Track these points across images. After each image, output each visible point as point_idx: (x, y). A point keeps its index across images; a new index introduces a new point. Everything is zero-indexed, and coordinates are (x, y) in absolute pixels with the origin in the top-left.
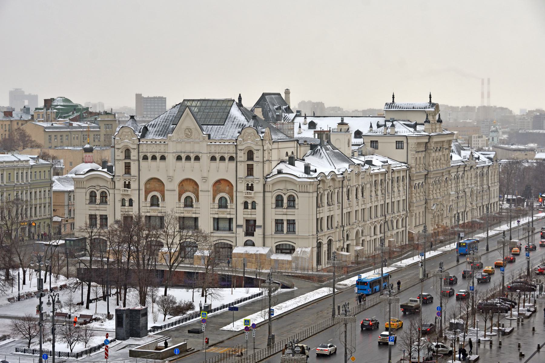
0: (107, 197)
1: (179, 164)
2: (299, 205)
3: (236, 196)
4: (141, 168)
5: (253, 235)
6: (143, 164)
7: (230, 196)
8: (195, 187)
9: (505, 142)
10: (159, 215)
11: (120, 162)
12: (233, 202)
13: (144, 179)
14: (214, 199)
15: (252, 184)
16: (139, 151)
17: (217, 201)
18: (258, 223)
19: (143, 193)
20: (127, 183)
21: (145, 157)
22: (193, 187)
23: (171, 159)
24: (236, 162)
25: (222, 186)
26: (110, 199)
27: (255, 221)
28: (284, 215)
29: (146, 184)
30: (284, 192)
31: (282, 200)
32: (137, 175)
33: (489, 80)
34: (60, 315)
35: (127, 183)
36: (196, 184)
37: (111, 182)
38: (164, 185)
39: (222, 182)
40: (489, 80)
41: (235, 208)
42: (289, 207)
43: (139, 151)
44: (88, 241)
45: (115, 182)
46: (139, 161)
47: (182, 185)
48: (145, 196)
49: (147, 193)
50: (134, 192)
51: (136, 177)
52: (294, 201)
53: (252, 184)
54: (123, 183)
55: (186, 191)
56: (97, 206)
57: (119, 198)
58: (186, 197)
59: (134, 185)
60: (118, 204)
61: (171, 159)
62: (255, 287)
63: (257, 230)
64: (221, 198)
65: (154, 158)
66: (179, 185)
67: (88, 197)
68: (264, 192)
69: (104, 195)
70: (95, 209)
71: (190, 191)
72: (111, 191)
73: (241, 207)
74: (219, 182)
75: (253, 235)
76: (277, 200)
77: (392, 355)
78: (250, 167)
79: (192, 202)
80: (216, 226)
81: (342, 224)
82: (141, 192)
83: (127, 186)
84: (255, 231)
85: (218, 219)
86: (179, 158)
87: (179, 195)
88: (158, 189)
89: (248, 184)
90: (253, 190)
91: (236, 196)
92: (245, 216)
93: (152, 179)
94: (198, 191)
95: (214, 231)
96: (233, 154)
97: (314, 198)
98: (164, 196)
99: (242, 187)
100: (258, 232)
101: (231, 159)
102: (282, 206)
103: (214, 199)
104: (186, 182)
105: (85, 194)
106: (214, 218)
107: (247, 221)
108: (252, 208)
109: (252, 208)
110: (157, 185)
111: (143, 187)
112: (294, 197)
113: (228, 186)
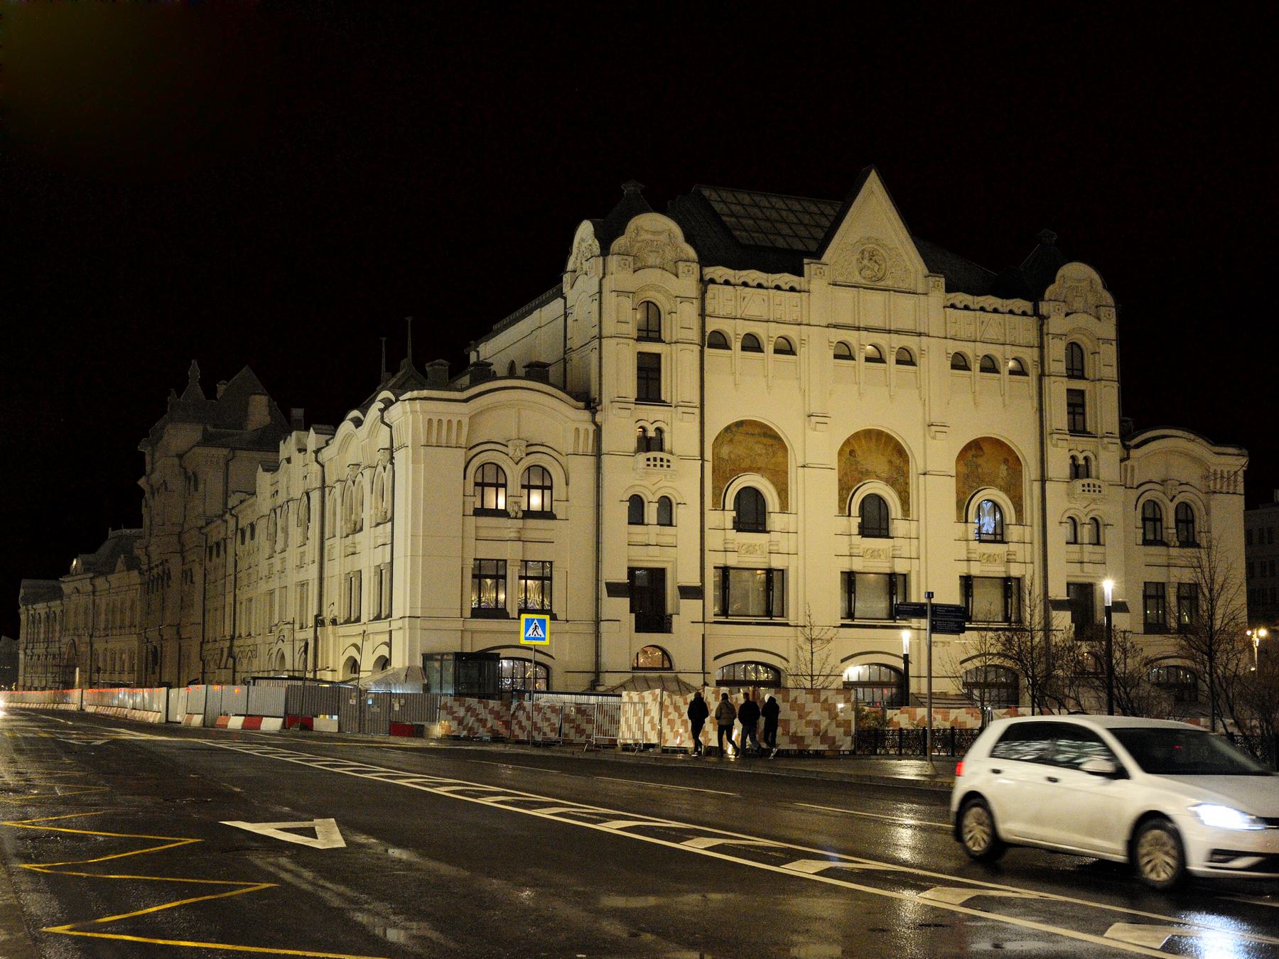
8: (897, 461)
9: (520, 371)
13: (717, 422)
16: (703, 308)
22: (890, 462)
25: (987, 464)
34: (636, 766)
36: (900, 451)
43: (703, 308)
44: (929, 605)
47: (852, 452)
49: (723, 474)
53: (659, 430)
55: (865, 474)
62: (1183, 774)
65: (752, 344)
66: (840, 453)
71: (878, 477)
74: (975, 447)
87: (841, 489)
88: (761, 462)
94: (905, 475)
97: (529, 535)
110: (759, 449)
113: (1006, 461)
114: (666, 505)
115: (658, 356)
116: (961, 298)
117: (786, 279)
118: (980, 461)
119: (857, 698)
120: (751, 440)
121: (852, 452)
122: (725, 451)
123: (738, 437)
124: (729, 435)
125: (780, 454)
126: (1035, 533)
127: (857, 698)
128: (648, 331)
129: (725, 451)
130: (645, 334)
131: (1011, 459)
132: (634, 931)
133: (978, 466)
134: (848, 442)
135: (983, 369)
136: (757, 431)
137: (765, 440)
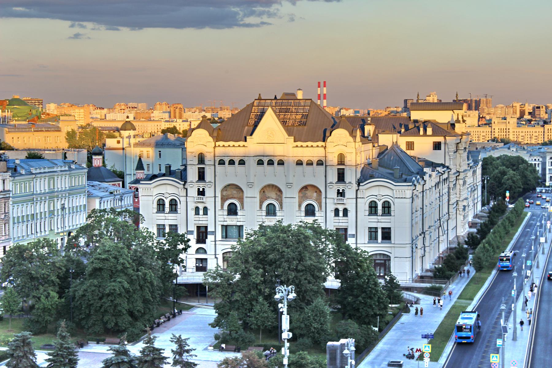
0: (177, 205)
1: (260, 167)
2: (395, 211)
3: (326, 203)
4: (216, 174)
5: (204, 242)
6: (219, 168)
7: (318, 203)
8: (279, 193)
10: (238, 225)
11: (194, 167)
12: (321, 208)
14: (300, 206)
15: (203, 189)
17: (303, 208)
18: (209, 229)
19: (219, 200)
20: (201, 190)
21: (270, 162)
22: (276, 194)
23: (252, 163)
24: (326, 166)
25: (309, 193)
26: (181, 207)
27: (206, 227)
28: (380, 222)
29: (222, 191)
30: (379, 198)
31: (164, 205)
32: (213, 181)
33: (325, 82)
35: (201, 190)
36: (280, 191)
37: (183, 189)
38: (242, 191)
39: (309, 188)
40: (325, 82)
41: (324, 216)
42: (384, 214)
45: (187, 189)
46: (215, 165)
47: (264, 192)
48: (221, 203)
49: (223, 200)
50: (208, 199)
51: (211, 184)
52: (176, 205)
53: (203, 189)
54: (197, 190)
56: (379, 217)
57: (192, 206)
58: (268, 204)
59: (209, 192)
60: (192, 213)
61: (252, 163)
63: (208, 236)
64: (230, 204)
66: (260, 192)
67: (155, 205)
68: (357, 198)
69: (174, 203)
70: (164, 218)
71: (272, 198)
72: (183, 199)
73: (331, 214)
74: (305, 188)
75: (204, 242)
76: (370, 207)
77: (505, 363)
78: (202, 171)
79: (236, 209)
80: (224, 234)
81: (423, 230)
82: (217, 198)
83: (201, 193)
84: (206, 238)
85: (226, 226)
86: (260, 163)
87: (260, 202)
88: (235, 196)
89: (199, 189)
90: (204, 195)
91: (326, 203)
92: (197, 222)
93: (229, 185)
94: (281, 197)
95: (223, 239)
96: (322, 158)
98: (243, 204)
99: (332, 193)
100: (210, 238)
101: (320, 163)
102: (164, 210)
103: (300, 206)
104: (268, 188)
105: (152, 202)
106: (222, 226)
107: (198, 228)
108: (204, 214)
109: (204, 214)
110: (235, 192)
111: (219, 194)
112: (176, 200)
113: (316, 192)
114: (205, 209)
115: (204, 168)
116: (299, 144)
117: (242, 143)
118: (307, 192)
119: (121, 202)
120: (232, 190)
121: (264, 192)
122: (225, 193)
123: (228, 189)
124: (225, 189)
125: (241, 193)
126: (323, 214)
127: (121, 202)
128: (341, 162)
129: (225, 193)
130: (340, 163)
131: (318, 191)
132: (155, 283)
133: (306, 194)
134: (263, 189)
135: (239, 164)
136: (234, 187)
137: (237, 190)
